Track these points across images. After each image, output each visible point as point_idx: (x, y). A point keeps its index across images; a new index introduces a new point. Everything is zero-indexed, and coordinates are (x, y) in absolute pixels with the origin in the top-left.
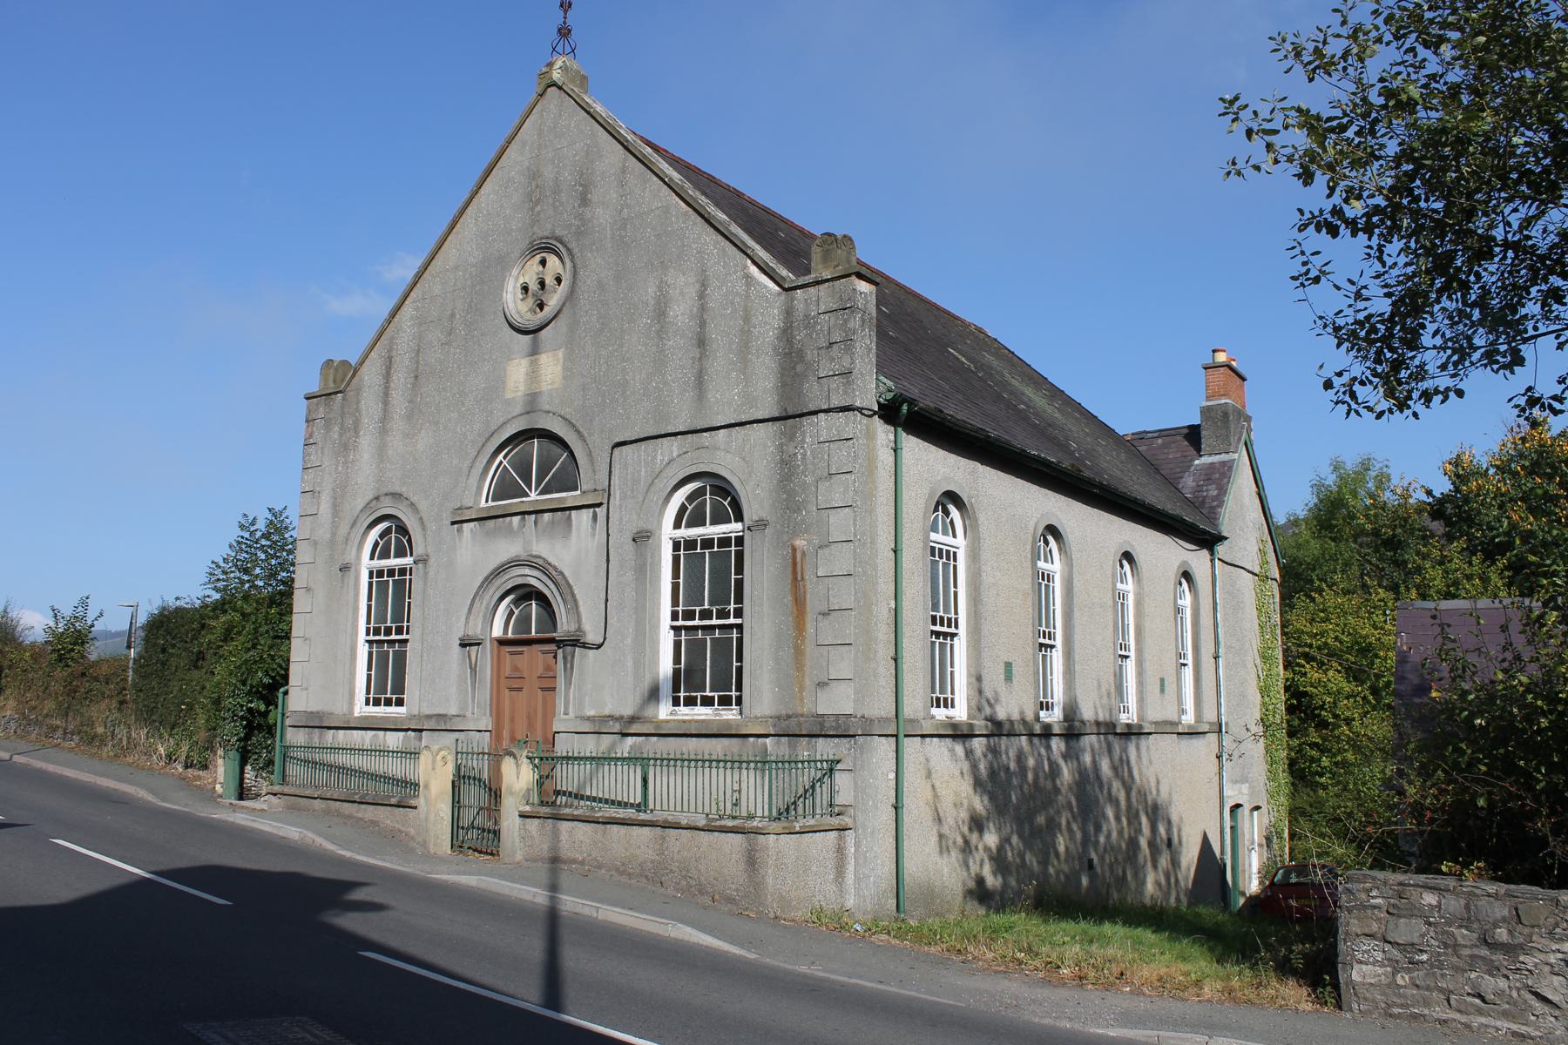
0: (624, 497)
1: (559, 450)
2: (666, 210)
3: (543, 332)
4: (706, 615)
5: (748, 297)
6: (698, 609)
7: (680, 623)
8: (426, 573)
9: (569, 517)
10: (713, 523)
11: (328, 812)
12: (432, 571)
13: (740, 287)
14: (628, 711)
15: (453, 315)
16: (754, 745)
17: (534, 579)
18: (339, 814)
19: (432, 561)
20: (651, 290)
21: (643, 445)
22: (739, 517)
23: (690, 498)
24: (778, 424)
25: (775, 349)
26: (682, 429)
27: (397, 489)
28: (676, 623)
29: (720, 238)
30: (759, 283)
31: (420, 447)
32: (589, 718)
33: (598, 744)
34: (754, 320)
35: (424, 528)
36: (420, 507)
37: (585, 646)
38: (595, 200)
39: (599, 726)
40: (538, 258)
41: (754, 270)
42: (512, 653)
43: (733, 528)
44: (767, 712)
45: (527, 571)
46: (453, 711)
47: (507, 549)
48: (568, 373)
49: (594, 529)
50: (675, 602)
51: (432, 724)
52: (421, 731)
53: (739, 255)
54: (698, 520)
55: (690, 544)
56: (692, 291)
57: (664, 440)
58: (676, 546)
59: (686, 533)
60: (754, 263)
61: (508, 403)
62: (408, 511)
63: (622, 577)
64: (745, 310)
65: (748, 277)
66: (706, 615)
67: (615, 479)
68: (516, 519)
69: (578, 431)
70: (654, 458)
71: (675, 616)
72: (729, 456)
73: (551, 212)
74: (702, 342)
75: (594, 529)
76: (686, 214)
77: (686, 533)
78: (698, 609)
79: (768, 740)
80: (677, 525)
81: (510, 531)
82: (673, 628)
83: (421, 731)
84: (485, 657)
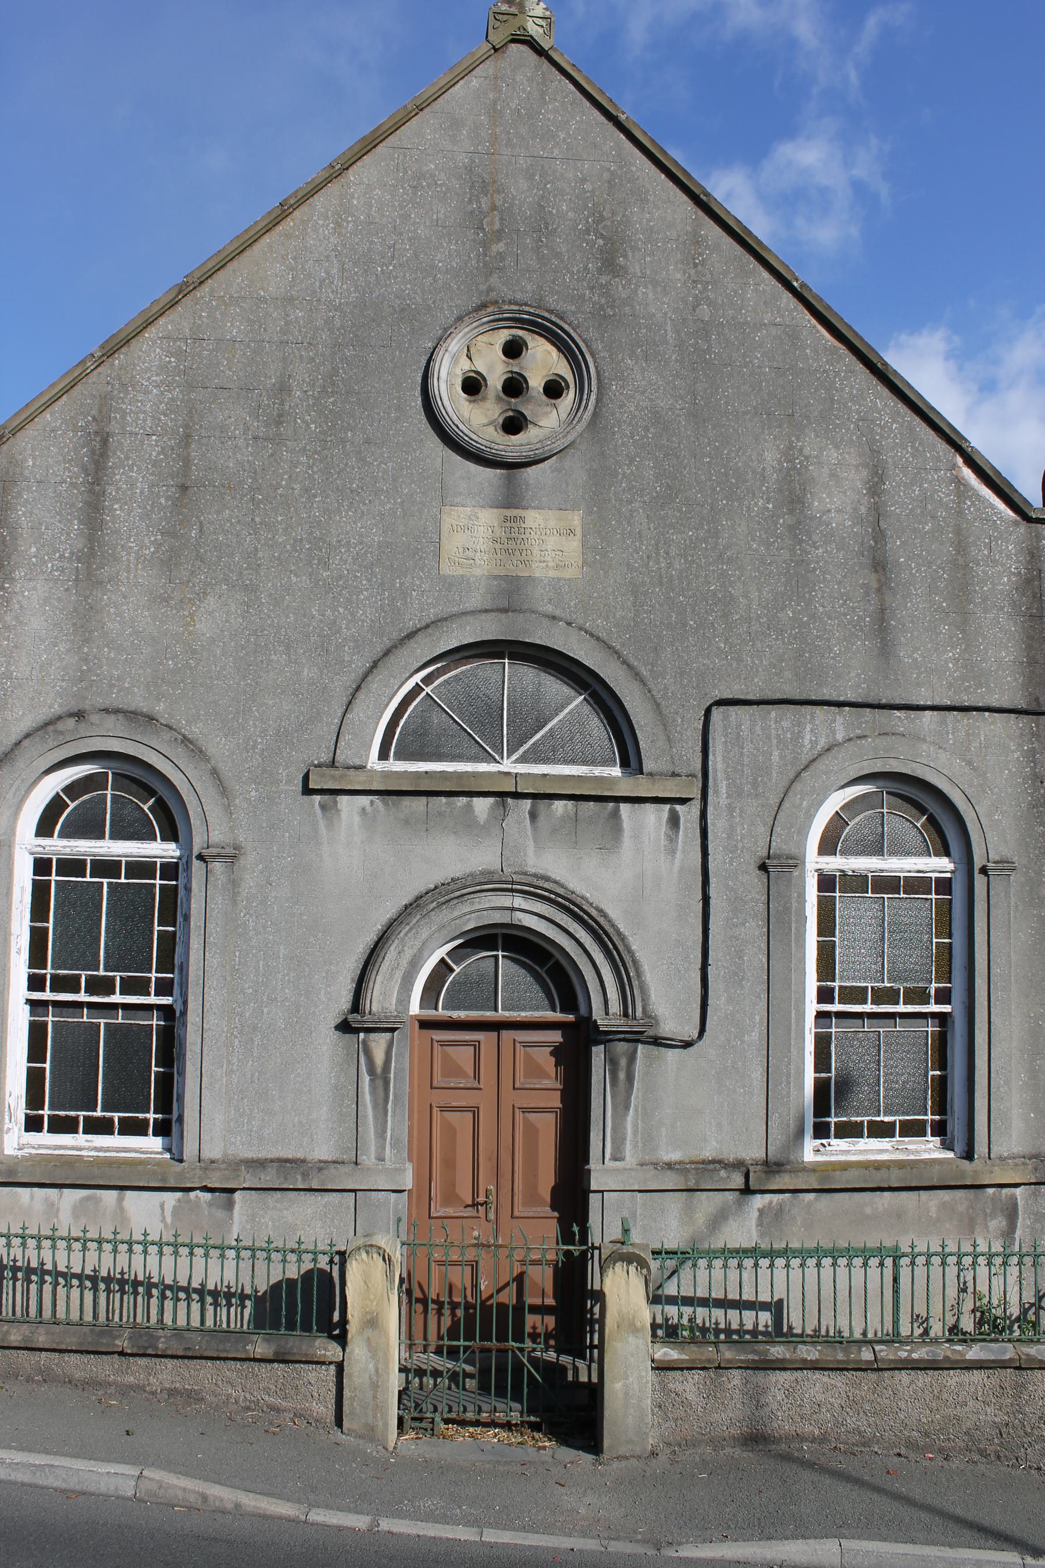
0: (736, 792)
1: (566, 690)
2: (794, 334)
3: (531, 471)
4: (97, 986)
5: (960, 513)
6: (84, 975)
7: (47, 995)
8: (234, 884)
9: (616, 814)
10: (114, 836)
11: (48, 1377)
12: (250, 882)
13: (945, 494)
14: (754, 1152)
15: (283, 389)
16: (993, 1199)
17: (531, 916)
18: (48, 1377)
19: (249, 859)
20: (771, 457)
21: (774, 712)
22: (171, 834)
23: (73, 789)
24: (1026, 718)
25: (1014, 604)
26: (851, 696)
27: (139, 701)
28: (37, 996)
29: (902, 408)
30: (978, 497)
31: (204, 627)
32: (670, 1166)
33: (688, 1211)
34: (973, 551)
35: (223, 790)
36: (211, 750)
37: (657, 1042)
38: (636, 269)
39: (696, 1177)
40: (504, 335)
41: (968, 473)
42: (443, 1044)
43: (160, 850)
44: (1017, 1149)
45: (519, 902)
46: (322, 1152)
47: (453, 854)
48: (595, 553)
49: (672, 840)
50: (37, 956)
51: (269, 1178)
52: (232, 1191)
53: (942, 446)
54: (87, 826)
55: (72, 866)
56: (856, 478)
57: (818, 710)
58: (41, 866)
59: (58, 846)
60: (971, 462)
61: (450, 584)
62: (179, 754)
63: (737, 930)
64: (958, 532)
65: (959, 481)
66: (103, 986)
67: (716, 761)
68: (482, 806)
69: (630, 667)
70: (800, 735)
71: (35, 983)
72: (943, 756)
73: (533, 263)
74: (879, 565)
75: (672, 840)
76: (833, 351)
77: (58, 846)
78: (84, 975)
79: (1018, 1191)
80: (44, 828)
81: (468, 824)
82: (30, 1002)
83: (232, 1191)
84: (401, 1056)
